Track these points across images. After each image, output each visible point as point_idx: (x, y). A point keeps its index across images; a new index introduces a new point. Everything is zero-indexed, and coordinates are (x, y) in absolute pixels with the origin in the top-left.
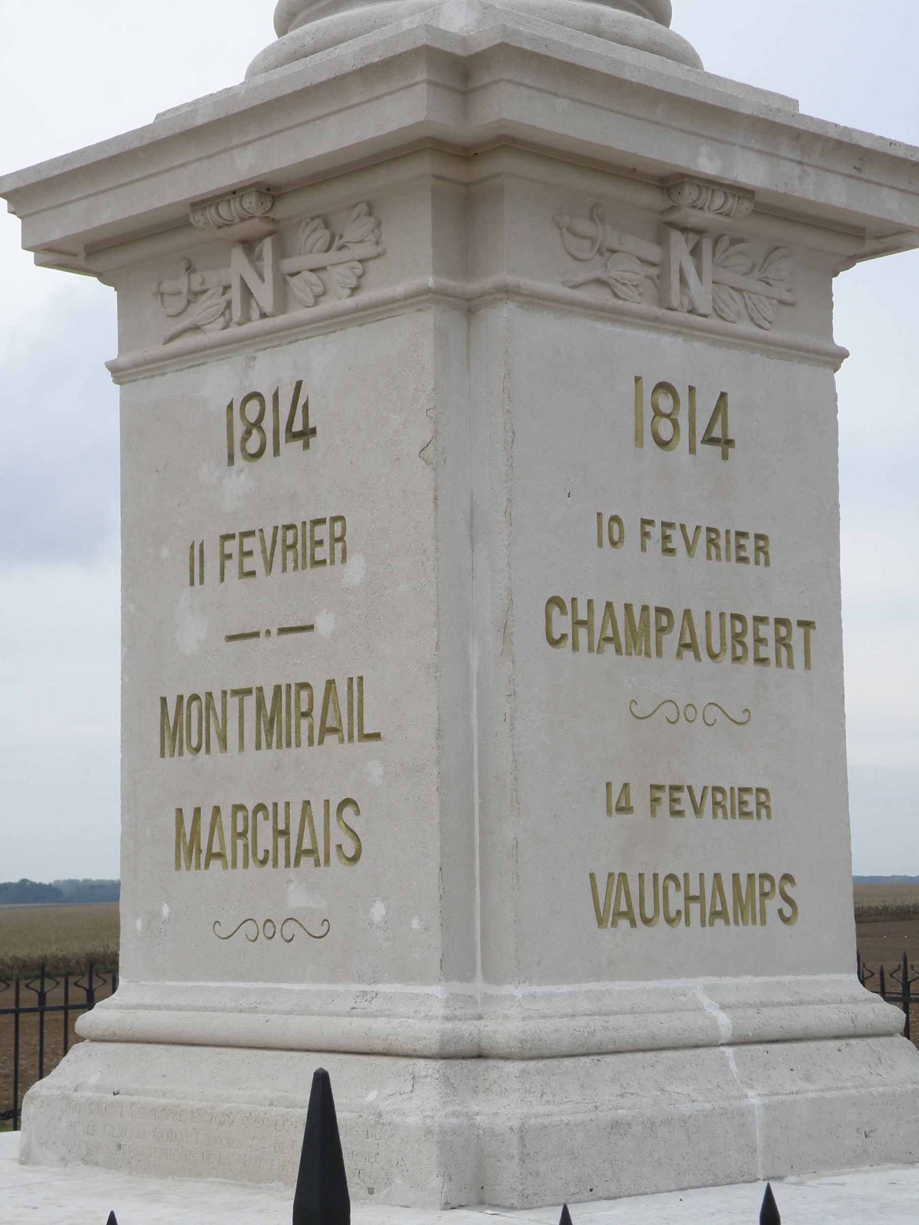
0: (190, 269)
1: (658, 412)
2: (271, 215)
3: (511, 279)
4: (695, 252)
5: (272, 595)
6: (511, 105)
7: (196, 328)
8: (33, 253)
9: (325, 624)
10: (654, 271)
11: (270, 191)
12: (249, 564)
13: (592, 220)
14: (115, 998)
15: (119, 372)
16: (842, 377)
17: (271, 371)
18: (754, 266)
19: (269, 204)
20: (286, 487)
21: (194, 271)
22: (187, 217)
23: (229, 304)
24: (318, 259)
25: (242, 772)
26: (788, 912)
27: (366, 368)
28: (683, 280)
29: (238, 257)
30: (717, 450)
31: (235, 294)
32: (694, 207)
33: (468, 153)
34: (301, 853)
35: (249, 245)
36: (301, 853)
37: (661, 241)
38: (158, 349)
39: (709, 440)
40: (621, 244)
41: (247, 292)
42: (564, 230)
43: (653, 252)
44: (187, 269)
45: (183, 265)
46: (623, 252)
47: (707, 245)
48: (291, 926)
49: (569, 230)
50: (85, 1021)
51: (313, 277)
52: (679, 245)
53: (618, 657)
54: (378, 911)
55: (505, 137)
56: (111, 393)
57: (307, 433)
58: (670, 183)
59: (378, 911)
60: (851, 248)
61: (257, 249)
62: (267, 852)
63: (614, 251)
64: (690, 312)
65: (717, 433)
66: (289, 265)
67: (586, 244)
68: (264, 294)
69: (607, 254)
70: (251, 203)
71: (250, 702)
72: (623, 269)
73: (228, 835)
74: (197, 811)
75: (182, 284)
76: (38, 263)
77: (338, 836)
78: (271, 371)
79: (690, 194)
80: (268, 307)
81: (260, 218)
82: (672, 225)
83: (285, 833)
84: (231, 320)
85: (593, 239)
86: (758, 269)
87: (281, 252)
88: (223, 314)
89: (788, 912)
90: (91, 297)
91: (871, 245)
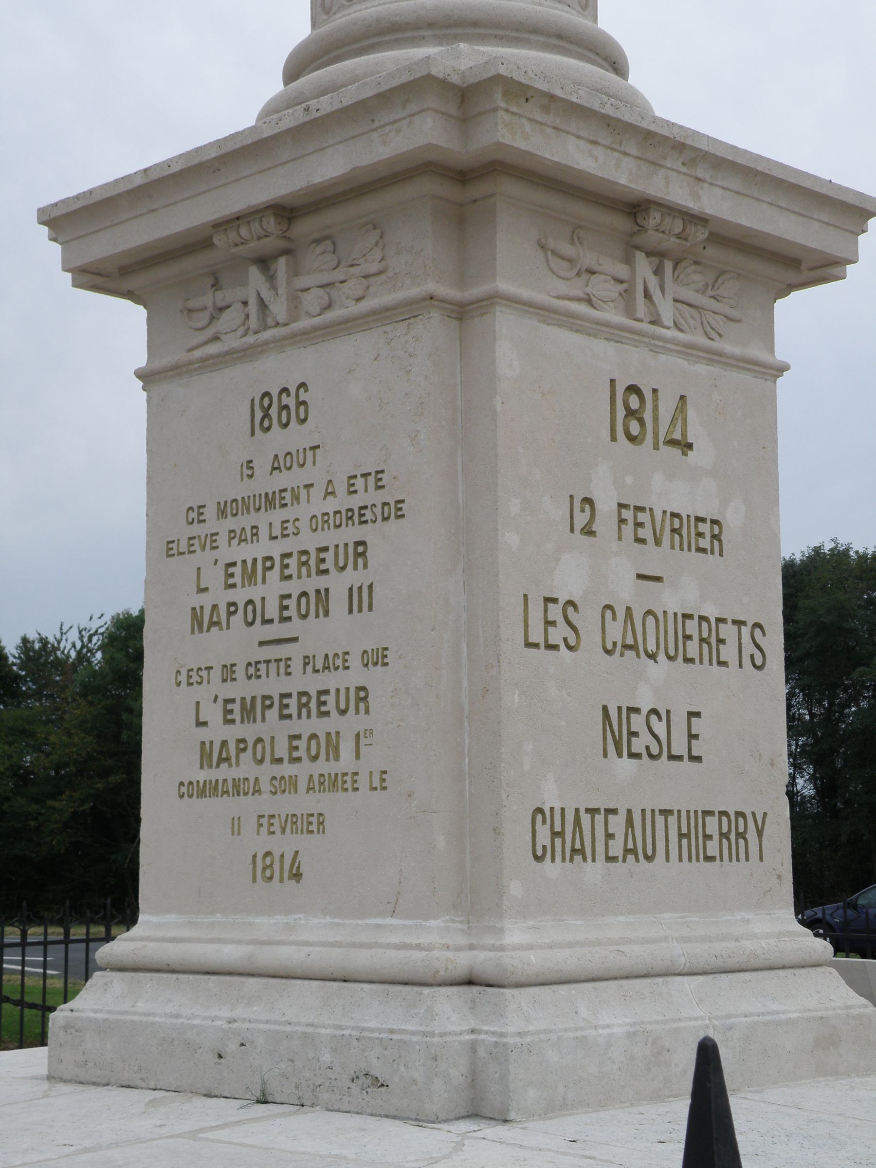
0: (216, 285)
2: (287, 234)
4: (658, 272)
7: (216, 338)
8: (70, 274)
10: (622, 287)
11: (286, 212)
13: (572, 243)
14: (135, 931)
15: (146, 377)
16: (142, 361)
17: (276, 371)
18: (707, 285)
19: (286, 226)
21: (220, 289)
22: (210, 238)
23: (247, 316)
28: (647, 295)
29: (255, 274)
30: (676, 452)
31: (253, 308)
32: (657, 230)
33: (463, 176)
35: (264, 262)
37: (628, 260)
38: (182, 356)
39: (672, 442)
40: (600, 265)
41: (263, 305)
42: (549, 253)
43: (622, 271)
44: (213, 286)
45: (210, 281)
46: (600, 273)
47: (668, 265)
49: (554, 252)
50: (105, 952)
51: (320, 292)
52: (644, 267)
53: (346, 478)
55: (495, 162)
56: (137, 397)
58: (636, 208)
60: (791, 276)
61: (273, 267)
62: (544, 847)
63: (593, 273)
64: (652, 323)
65: (677, 436)
66: (303, 281)
67: (565, 264)
68: (279, 309)
69: (585, 276)
70: (271, 224)
72: (602, 287)
75: (207, 300)
76: (76, 284)
78: (276, 371)
79: (654, 218)
80: (282, 317)
81: (278, 236)
82: (637, 247)
83: (561, 834)
84: (249, 329)
85: (570, 260)
86: (711, 286)
87: (295, 272)
88: (244, 324)
91: (806, 275)
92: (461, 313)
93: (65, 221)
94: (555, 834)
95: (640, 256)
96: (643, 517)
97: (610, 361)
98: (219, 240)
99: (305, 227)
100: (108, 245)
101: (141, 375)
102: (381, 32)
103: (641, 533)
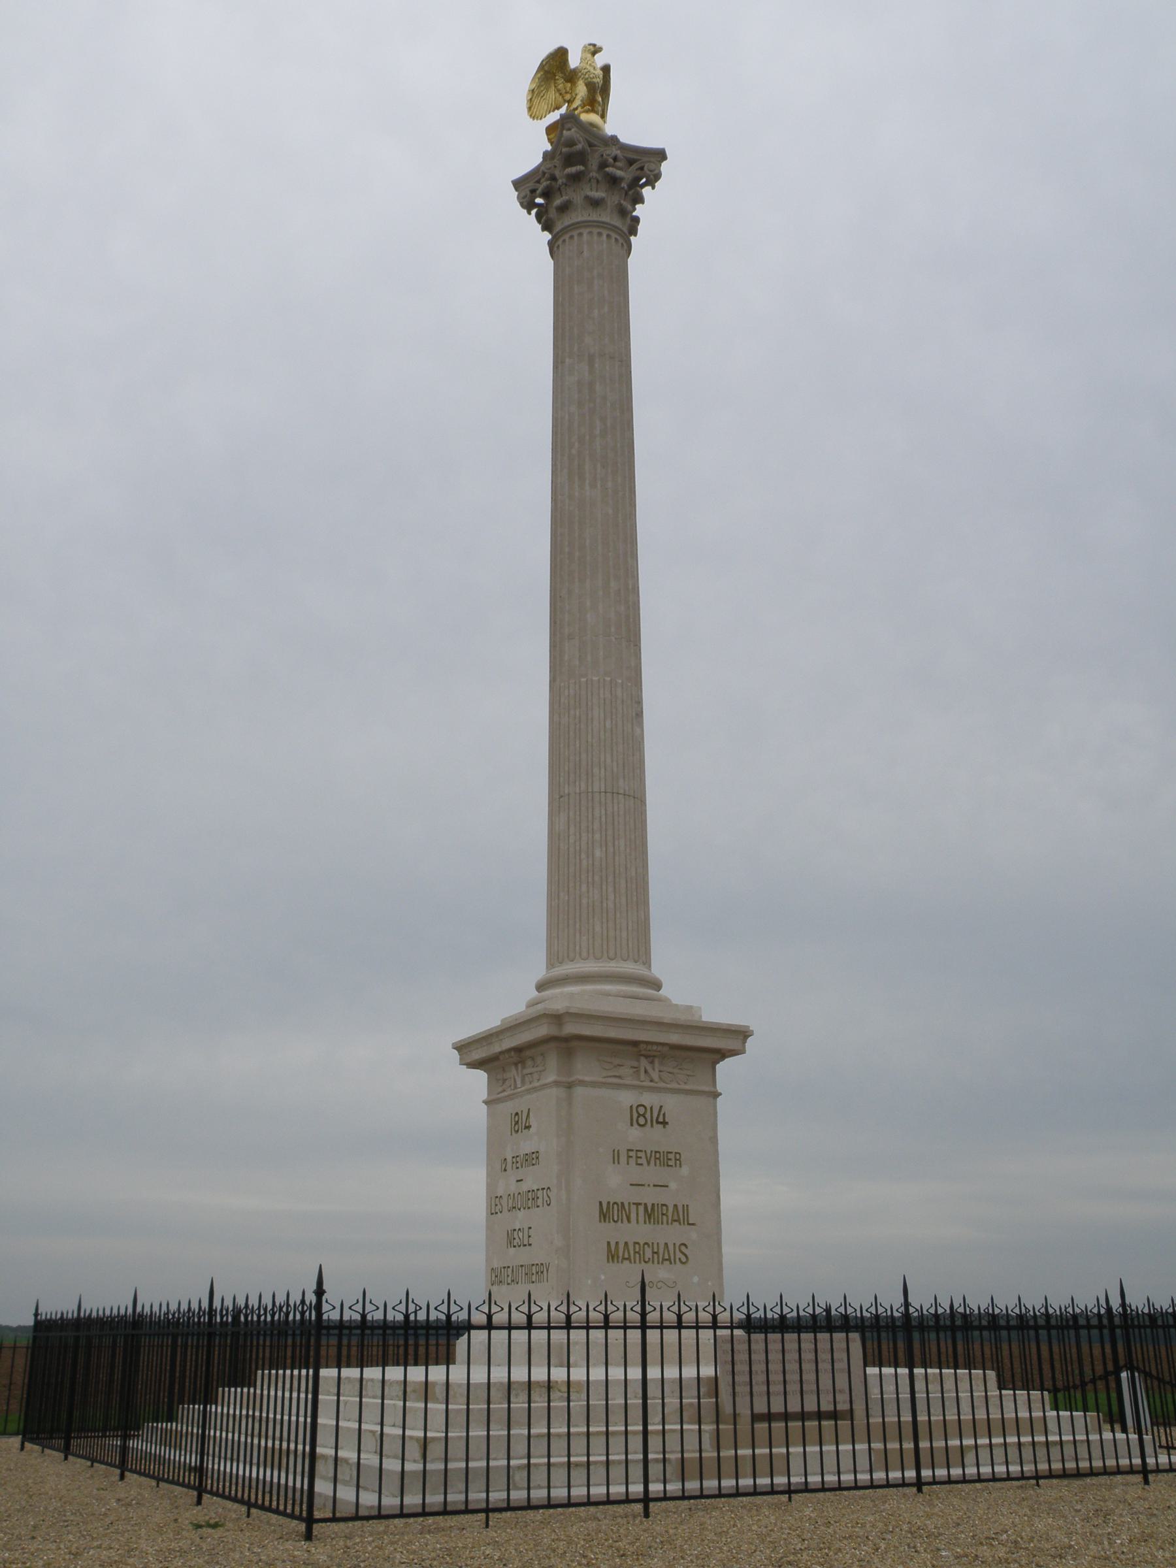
1: (644, 1116)
3: (580, 1077)
5: (652, 1173)
6: (570, 1029)
9: (673, 1185)
11: (518, 1050)
12: (640, 1161)
16: (485, 1096)
20: (653, 1139)
24: (671, 1070)
25: (637, 1231)
26: (684, 1259)
27: (542, 1098)
28: (646, 1072)
29: (513, 1068)
34: (664, 1260)
35: (516, 1064)
36: (664, 1260)
37: (638, 1061)
39: (658, 1122)
43: (635, 1064)
48: (660, 1285)
52: (644, 1062)
54: (696, 1279)
57: (665, 1123)
58: (635, 1043)
59: (696, 1279)
65: (661, 1119)
71: (641, 1208)
73: (632, 1252)
74: (617, 1243)
77: (679, 1255)
87: (524, 1067)
89: (684, 1259)
90: (480, 1077)
92: (570, 1086)
93: (462, 1048)
94: (654, 1253)
95: (642, 1058)
96: (639, 1154)
97: (627, 1098)
98: (501, 1058)
99: (528, 1053)
100: (478, 1054)
101: (486, 1102)
102: (607, 977)
103: (640, 1161)
